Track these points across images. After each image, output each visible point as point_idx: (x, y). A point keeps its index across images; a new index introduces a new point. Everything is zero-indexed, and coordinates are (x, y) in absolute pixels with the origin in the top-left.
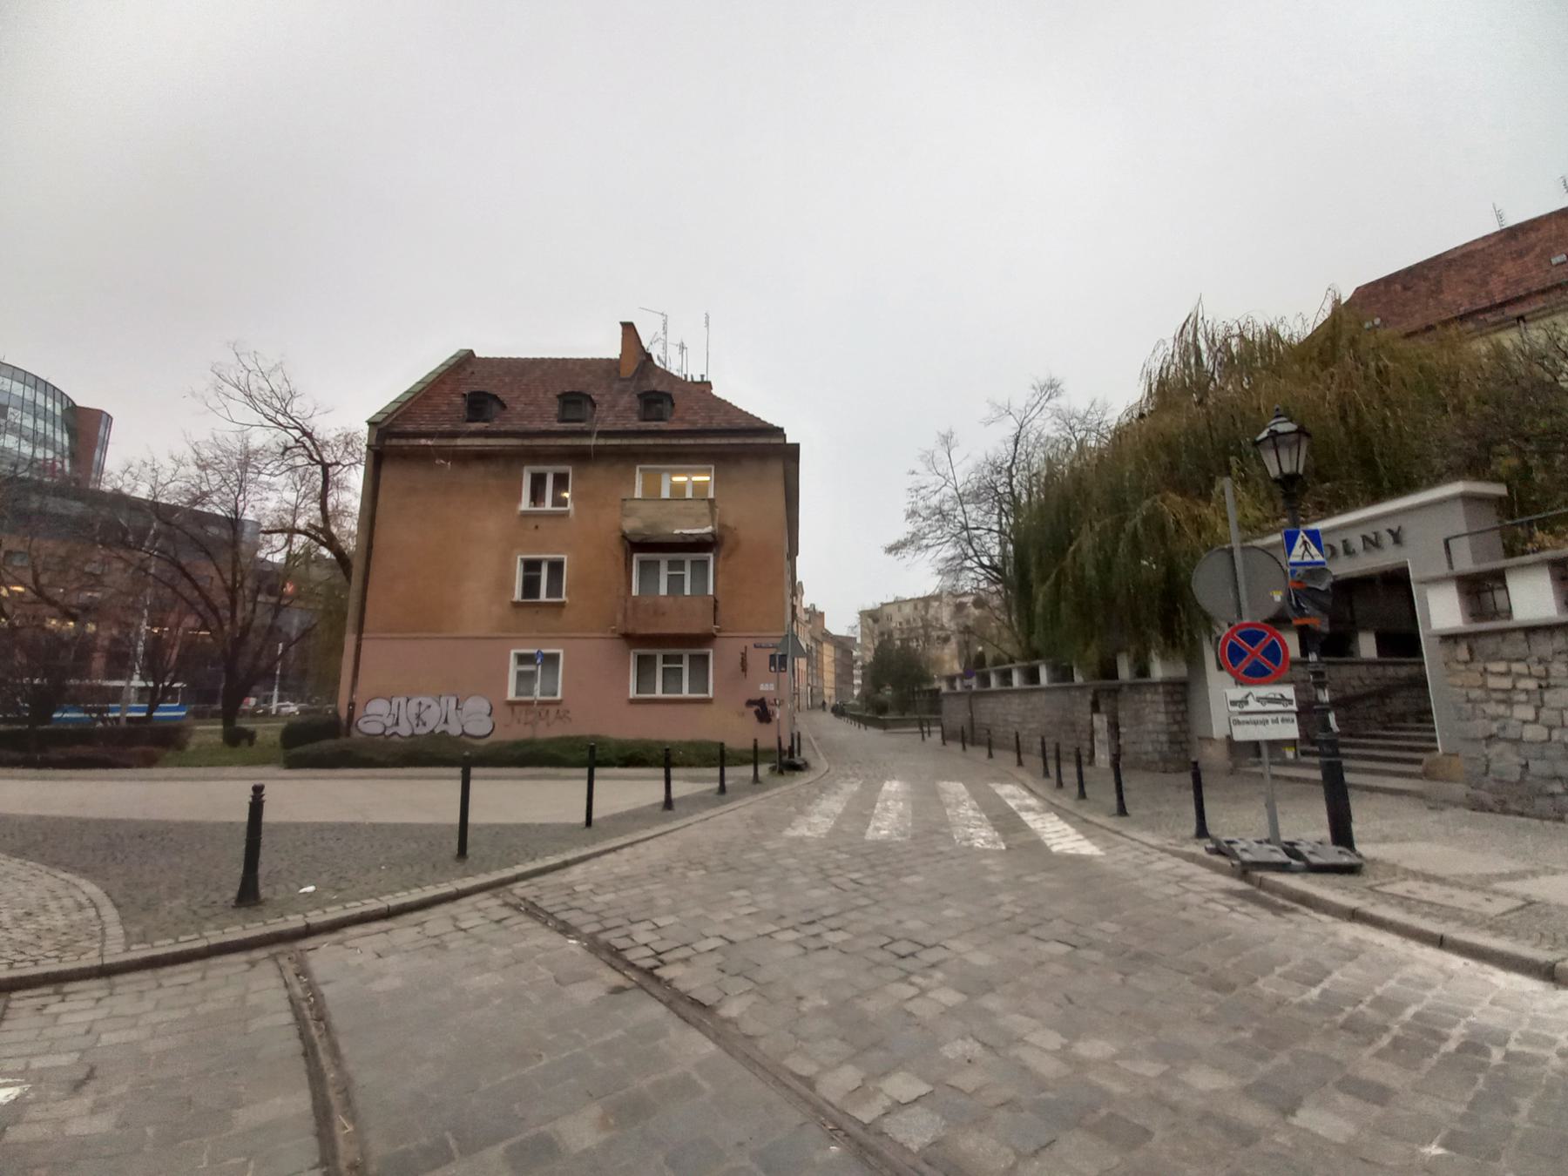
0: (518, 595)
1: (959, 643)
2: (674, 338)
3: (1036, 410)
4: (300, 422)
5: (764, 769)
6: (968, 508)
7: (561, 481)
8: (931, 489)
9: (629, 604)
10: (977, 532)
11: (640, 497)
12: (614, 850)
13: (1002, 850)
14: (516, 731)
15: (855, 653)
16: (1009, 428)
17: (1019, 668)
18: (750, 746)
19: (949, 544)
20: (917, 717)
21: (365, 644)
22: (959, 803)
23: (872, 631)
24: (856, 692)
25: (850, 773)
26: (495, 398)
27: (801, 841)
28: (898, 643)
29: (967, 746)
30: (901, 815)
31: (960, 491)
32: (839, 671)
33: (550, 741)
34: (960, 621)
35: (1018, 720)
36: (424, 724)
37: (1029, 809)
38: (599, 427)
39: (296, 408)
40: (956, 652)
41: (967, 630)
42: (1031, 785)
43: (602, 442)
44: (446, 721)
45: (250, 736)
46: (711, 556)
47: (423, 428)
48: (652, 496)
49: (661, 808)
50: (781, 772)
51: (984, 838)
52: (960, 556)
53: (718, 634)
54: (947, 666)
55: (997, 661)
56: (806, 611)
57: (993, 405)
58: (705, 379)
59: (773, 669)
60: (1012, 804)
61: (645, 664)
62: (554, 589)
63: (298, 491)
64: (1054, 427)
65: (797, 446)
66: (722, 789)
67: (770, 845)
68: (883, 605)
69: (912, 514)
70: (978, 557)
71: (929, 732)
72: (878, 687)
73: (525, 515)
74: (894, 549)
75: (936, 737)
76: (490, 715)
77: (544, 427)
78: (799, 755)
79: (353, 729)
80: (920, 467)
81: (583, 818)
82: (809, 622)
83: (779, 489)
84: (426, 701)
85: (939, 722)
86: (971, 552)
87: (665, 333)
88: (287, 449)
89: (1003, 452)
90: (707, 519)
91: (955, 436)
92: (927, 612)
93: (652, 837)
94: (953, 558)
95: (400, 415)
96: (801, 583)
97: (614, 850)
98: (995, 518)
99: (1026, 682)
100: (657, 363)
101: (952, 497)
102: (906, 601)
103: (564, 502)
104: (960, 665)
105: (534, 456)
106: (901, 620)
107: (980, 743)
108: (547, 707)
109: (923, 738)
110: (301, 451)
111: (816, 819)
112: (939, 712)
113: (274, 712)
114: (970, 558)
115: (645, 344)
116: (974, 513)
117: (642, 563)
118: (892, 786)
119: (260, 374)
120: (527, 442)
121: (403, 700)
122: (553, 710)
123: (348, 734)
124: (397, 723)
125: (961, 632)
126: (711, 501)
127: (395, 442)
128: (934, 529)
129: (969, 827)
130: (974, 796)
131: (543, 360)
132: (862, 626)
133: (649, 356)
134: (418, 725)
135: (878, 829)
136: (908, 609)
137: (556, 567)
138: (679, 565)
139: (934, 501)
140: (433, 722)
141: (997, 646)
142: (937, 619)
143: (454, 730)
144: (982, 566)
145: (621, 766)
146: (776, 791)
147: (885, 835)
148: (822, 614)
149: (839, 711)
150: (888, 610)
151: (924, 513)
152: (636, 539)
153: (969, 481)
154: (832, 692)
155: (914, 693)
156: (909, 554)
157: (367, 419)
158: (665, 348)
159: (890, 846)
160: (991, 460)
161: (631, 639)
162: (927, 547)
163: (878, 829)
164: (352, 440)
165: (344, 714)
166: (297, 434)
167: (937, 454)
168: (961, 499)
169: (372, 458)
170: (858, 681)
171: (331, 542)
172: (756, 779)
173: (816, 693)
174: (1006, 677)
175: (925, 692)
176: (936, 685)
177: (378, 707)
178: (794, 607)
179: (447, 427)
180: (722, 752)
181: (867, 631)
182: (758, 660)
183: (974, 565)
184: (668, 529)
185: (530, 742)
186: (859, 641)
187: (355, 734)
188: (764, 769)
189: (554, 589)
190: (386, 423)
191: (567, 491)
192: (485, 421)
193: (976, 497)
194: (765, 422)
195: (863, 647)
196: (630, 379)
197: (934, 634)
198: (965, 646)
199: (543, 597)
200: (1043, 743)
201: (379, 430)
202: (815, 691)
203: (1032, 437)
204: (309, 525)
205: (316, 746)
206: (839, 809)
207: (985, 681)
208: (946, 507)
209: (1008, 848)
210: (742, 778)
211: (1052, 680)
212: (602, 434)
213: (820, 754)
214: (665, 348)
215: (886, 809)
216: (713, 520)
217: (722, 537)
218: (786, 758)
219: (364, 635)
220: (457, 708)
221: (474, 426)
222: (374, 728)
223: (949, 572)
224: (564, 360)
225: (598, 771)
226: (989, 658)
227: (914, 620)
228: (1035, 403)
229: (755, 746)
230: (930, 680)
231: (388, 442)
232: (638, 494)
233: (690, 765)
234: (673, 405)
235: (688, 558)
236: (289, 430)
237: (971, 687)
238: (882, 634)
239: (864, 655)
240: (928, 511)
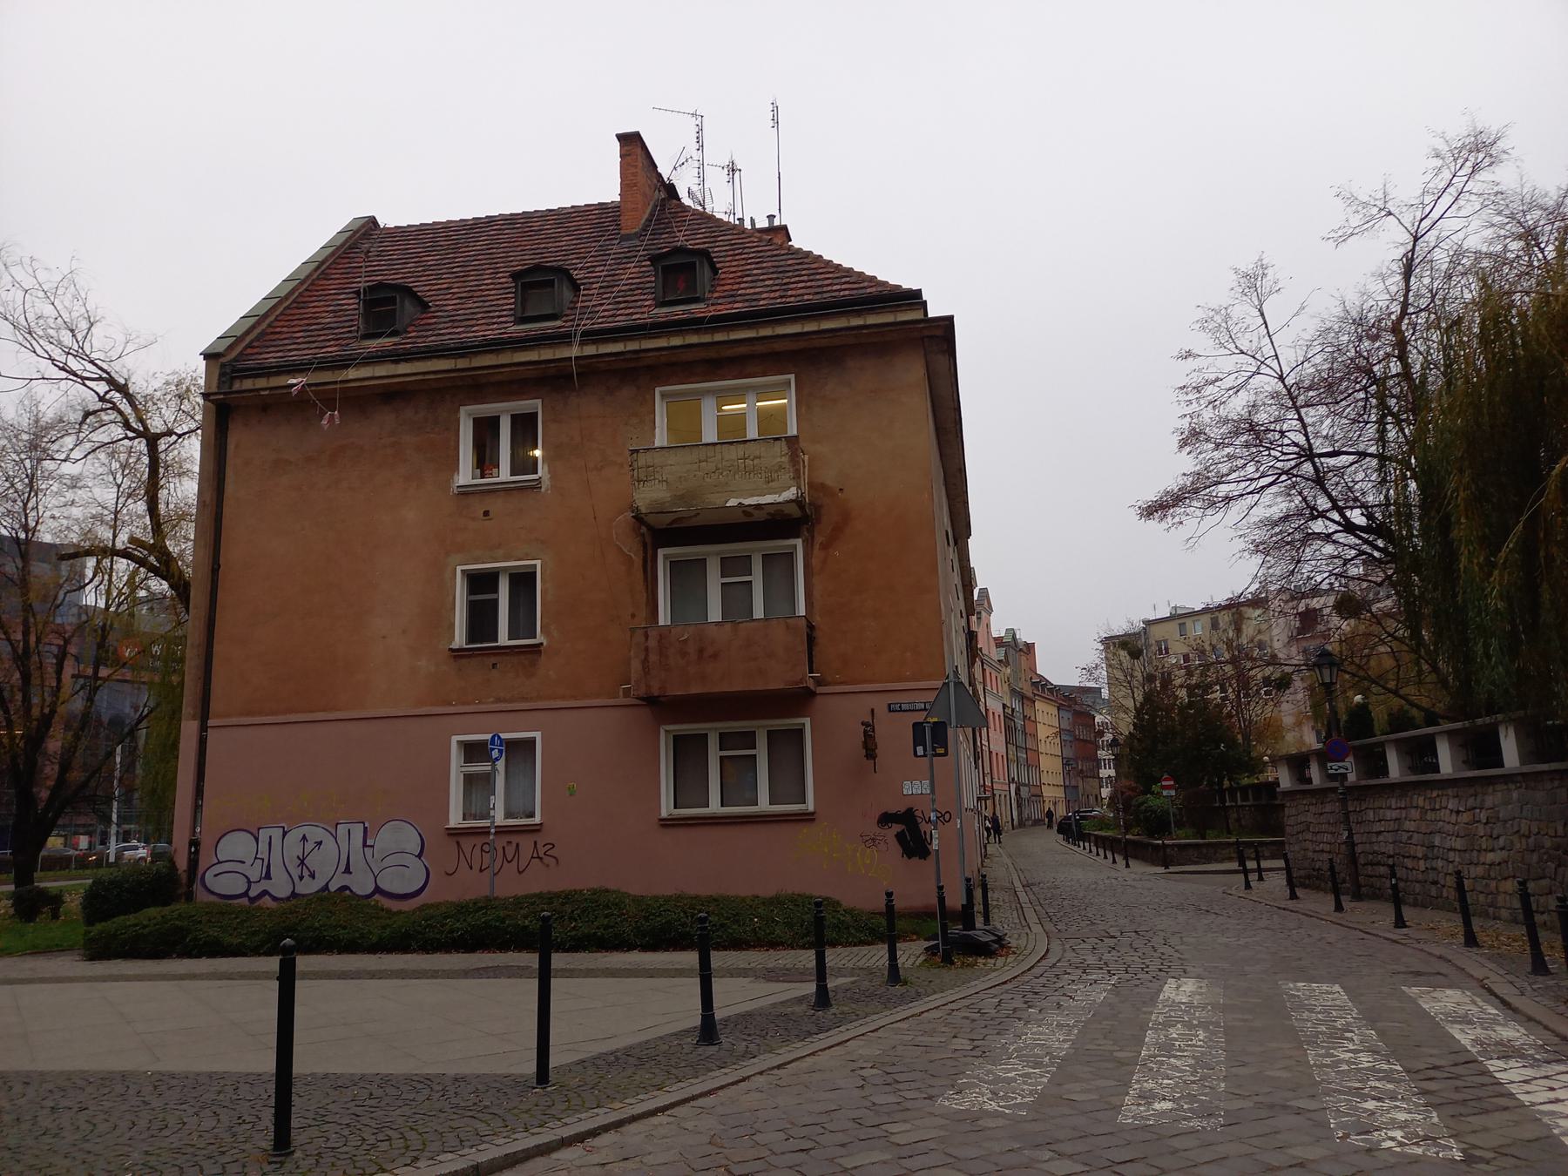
0: (459, 639)
1: (1311, 689)
2: (716, 154)
3: (1446, 200)
4: (105, 366)
5: (911, 953)
6: (1310, 415)
7: (525, 427)
8: (1229, 382)
9: (652, 643)
10: (1332, 461)
11: (665, 444)
12: (580, 1138)
13: (1453, 1160)
14: (467, 886)
15: (1099, 718)
16: (1389, 243)
17: (1450, 734)
18: (880, 904)
19: (1274, 489)
20: (1233, 840)
21: (212, 735)
22: (1337, 1036)
23: (1129, 674)
24: (1106, 792)
25: (1091, 960)
26: (408, 291)
27: (973, 1119)
28: (1182, 693)
29: (1346, 902)
30: (1199, 1062)
31: (1290, 381)
32: (1069, 753)
33: (518, 902)
34: (1312, 645)
35: (1458, 844)
36: (313, 876)
37: (1508, 1052)
38: (587, 325)
39: (98, 344)
40: (1307, 708)
41: (1324, 660)
42: (1504, 990)
43: (590, 350)
44: (347, 870)
45: (55, 900)
46: (799, 542)
47: (294, 356)
48: (687, 440)
49: (691, 1040)
50: (947, 960)
51: (1403, 1126)
52: (1300, 514)
53: (820, 690)
54: (1290, 737)
55: (1399, 722)
56: (999, 642)
57: (1351, 200)
58: (776, 223)
59: (920, 750)
60: (1464, 1037)
61: (688, 753)
62: (522, 621)
63: (119, 486)
64: (1489, 233)
65: (949, 320)
66: (823, 998)
67: (902, 1131)
68: (1148, 623)
69: (1193, 437)
70: (1341, 511)
71: (1259, 870)
72: (1147, 781)
73: (466, 493)
74: (1157, 509)
75: (1276, 882)
76: (419, 856)
77: (491, 333)
78: (987, 920)
79: (197, 887)
80: (1202, 343)
81: (531, 1068)
82: (1004, 662)
83: (918, 405)
84: (315, 833)
85: (1279, 851)
86: (1323, 503)
87: (701, 148)
88: (87, 414)
89: (1381, 296)
90: (786, 477)
91: (1270, 272)
92: (1238, 630)
93: (662, 1109)
94: (1286, 518)
95: (257, 339)
96: (984, 593)
97: (580, 1138)
98: (1371, 430)
99: (1413, 769)
100: (687, 201)
101: (1275, 395)
102: (1193, 614)
103: (532, 466)
104: (1318, 733)
105: (475, 387)
106: (1185, 650)
107: (1376, 896)
108: (515, 839)
109: (1248, 886)
110: (113, 415)
111: (1012, 1070)
112: (1279, 829)
113: (112, 859)
114: (1322, 515)
115: (664, 169)
116: (1324, 424)
117: (675, 566)
118: (1180, 991)
119: (41, 294)
120: (462, 363)
121: (276, 834)
122: (526, 843)
123: (190, 897)
124: (268, 876)
125: (1311, 668)
126: (792, 441)
127: (248, 384)
128: (1240, 462)
129: (1364, 1098)
130: (1371, 1018)
131: (490, 220)
132: (1109, 666)
133: (671, 190)
134: (301, 878)
135: (1147, 1097)
136: (1198, 629)
137: (523, 582)
138: (743, 564)
139: (1237, 406)
140: (326, 871)
141: (1396, 693)
142: (1261, 645)
143: (362, 885)
144: (1349, 527)
145: (646, 948)
146: (936, 999)
147: (1163, 1113)
148: (1030, 648)
149: (1072, 830)
150: (1157, 633)
151: (1216, 433)
152: (663, 521)
153: (1308, 360)
154: (1060, 793)
155: (1222, 792)
156: (1191, 518)
157: (204, 347)
158: (701, 177)
159: (1176, 1143)
160: (1354, 314)
161: (660, 707)
162: (1228, 499)
163: (1147, 1097)
164: (188, 390)
165: (182, 863)
166: (102, 388)
167: (1236, 312)
168: (1292, 397)
169: (212, 416)
170: (1107, 772)
171: (165, 566)
172: (894, 975)
173: (1027, 795)
174: (1421, 755)
175: (1244, 790)
176: (1270, 775)
177: (237, 846)
178: (971, 637)
179: (332, 350)
180: (819, 921)
181: (1119, 675)
182: (895, 734)
183: (1333, 527)
184: (716, 500)
185: (487, 904)
186: (1105, 693)
187: (201, 896)
188: (911, 953)
189: (522, 621)
190: (234, 354)
191: (536, 448)
192: (394, 334)
193: (1328, 388)
194: (885, 283)
195: (1114, 706)
196: (638, 236)
197: (1258, 674)
198: (1324, 693)
199: (503, 639)
200: (1525, 897)
201: (223, 366)
202: (1024, 792)
203: (1441, 258)
204: (132, 540)
205: (131, 919)
206: (1060, 1043)
207: (1374, 763)
208: (1261, 417)
209: (1469, 1159)
210: (869, 971)
211: (1525, 758)
212: (591, 336)
213: (1032, 917)
214: (701, 177)
215: (1167, 1048)
216: (797, 476)
217: (817, 508)
218: (956, 929)
219: (210, 723)
220: (365, 845)
221: (374, 344)
222: (230, 885)
223: (1278, 546)
224: (527, 216)
225: (558, 960)
226: (1379, 714)
227: (1214, 648)
228: (1442, 185)
229: (890, 906)
230: (1255, 766)
231: (237, 386)
232: (661, 438)
233: (774, 945)
234: (715, 271)
235: (756, 550)
236: (87, 382)
237: (1344, 776)
238: (1150, 678)
239: (1114, 721)
240: (1224, 429)
